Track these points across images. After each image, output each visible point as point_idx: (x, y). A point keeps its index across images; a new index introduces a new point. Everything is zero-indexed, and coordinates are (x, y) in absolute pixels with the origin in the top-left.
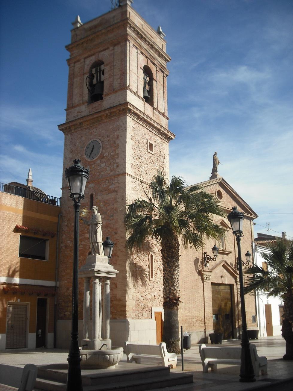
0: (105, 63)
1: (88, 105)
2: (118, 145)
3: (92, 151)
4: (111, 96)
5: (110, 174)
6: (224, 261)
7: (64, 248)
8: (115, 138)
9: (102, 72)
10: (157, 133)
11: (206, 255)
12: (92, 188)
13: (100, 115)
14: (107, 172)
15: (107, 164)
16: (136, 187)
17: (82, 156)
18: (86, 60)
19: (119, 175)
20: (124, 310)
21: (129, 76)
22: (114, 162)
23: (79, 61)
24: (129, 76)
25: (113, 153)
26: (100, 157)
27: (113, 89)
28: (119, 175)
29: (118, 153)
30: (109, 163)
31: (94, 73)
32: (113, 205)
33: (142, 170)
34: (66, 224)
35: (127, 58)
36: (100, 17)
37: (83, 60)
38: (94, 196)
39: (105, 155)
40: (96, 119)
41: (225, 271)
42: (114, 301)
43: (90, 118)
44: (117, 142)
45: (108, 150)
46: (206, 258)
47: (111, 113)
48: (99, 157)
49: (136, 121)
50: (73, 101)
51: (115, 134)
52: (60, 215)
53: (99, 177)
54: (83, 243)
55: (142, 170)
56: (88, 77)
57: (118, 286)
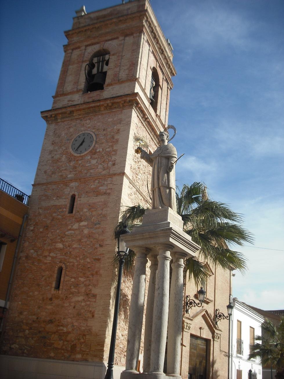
0: (111, 53)
1: (83, 94)
2: (117, 141)
3: (81, 144)
4: (114, 87)
5: (102, 173)
6: (205, 310)
7: (24, 259)
8: (114, 132)
9: (105, 62)
10: (158, 143)
11: (188, 299)
12: (75, 188)
13: (98, 104)
14: (98, 171)
15: (99, 161)
16: (131, 195)
17: (66, 149)
18: (88, 48)
19: (115, 175)
20: (101, 350)
21: (140, 68)
22: (109, 160)
23: (79, 48)
24: (140, 68)
25: (110, 149)
26: (91, 152)
27: (118, 79)
28: (115, 175)
29: (117, 150)
30: (103, 160)
31: (95, 63)
32: (102, 210)
33: (140, 178)
34: (32, 228)
35: (139, 50)
36: (111, 7)
37: (84, 48)
38: (77, 197)
39: (98, 150)
40: (91, 110)
41: (204, 322)
42: (87, 336)
43: (85, 106)
44: (116, 137)
45: (104, 145)
46: (189, 303)
47: (113, 103)
48: (90, 152)
49: (140, 120)
50: (64, 88)
51: (115, 128)
52: (25, 216)
53: (86, 175)
54: (52, 254)
55: (139, 177)
56: (87, 64)
57: (96, 316)
